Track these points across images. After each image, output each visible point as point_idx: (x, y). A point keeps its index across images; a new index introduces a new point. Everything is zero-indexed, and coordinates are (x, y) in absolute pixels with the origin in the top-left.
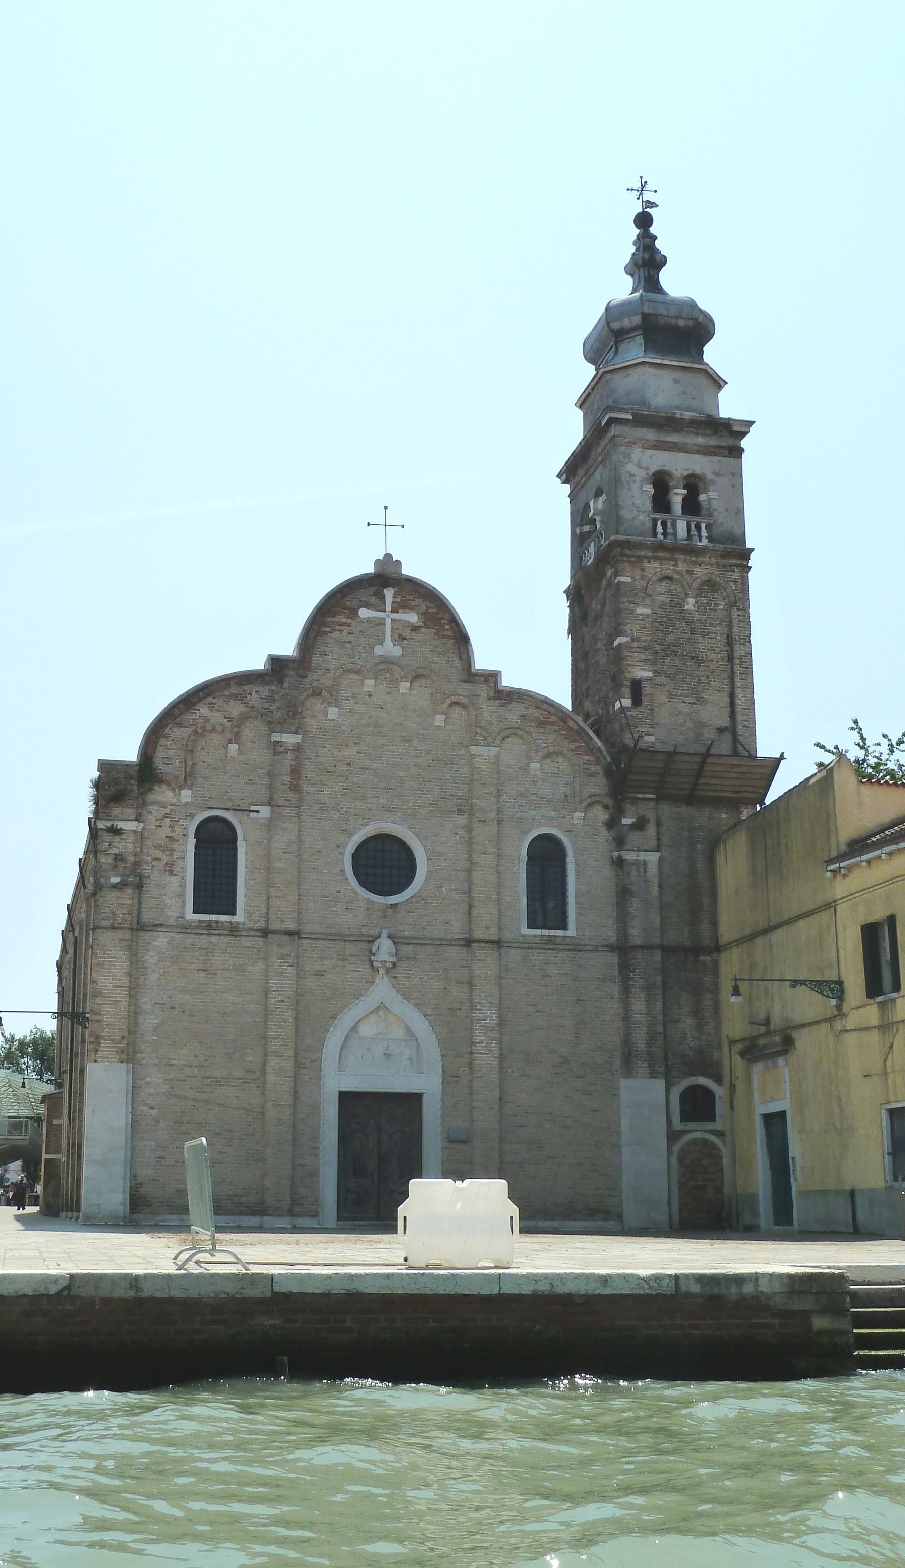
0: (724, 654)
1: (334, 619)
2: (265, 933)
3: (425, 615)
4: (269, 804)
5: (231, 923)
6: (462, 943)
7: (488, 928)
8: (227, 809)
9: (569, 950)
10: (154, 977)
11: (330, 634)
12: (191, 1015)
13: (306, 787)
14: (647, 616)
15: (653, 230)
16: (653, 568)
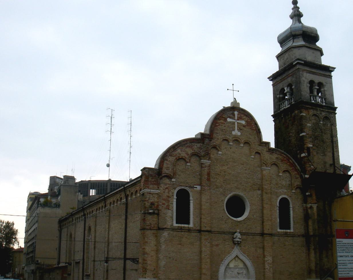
0: (330, 140)
1: (220, 121)
2: (200, 231)
3: (246, 121)
4: (200, 185)
5: (188, 227)
6: (260, 234)
7: (269, 229)
8: (187, 187)
9: (291, 237)
10: (163, 247)
11: (219, 127)
12: (176, 261)
13: (212, 180)
14: (310, 126)
15: (298, 5)
16: (312, 112)
